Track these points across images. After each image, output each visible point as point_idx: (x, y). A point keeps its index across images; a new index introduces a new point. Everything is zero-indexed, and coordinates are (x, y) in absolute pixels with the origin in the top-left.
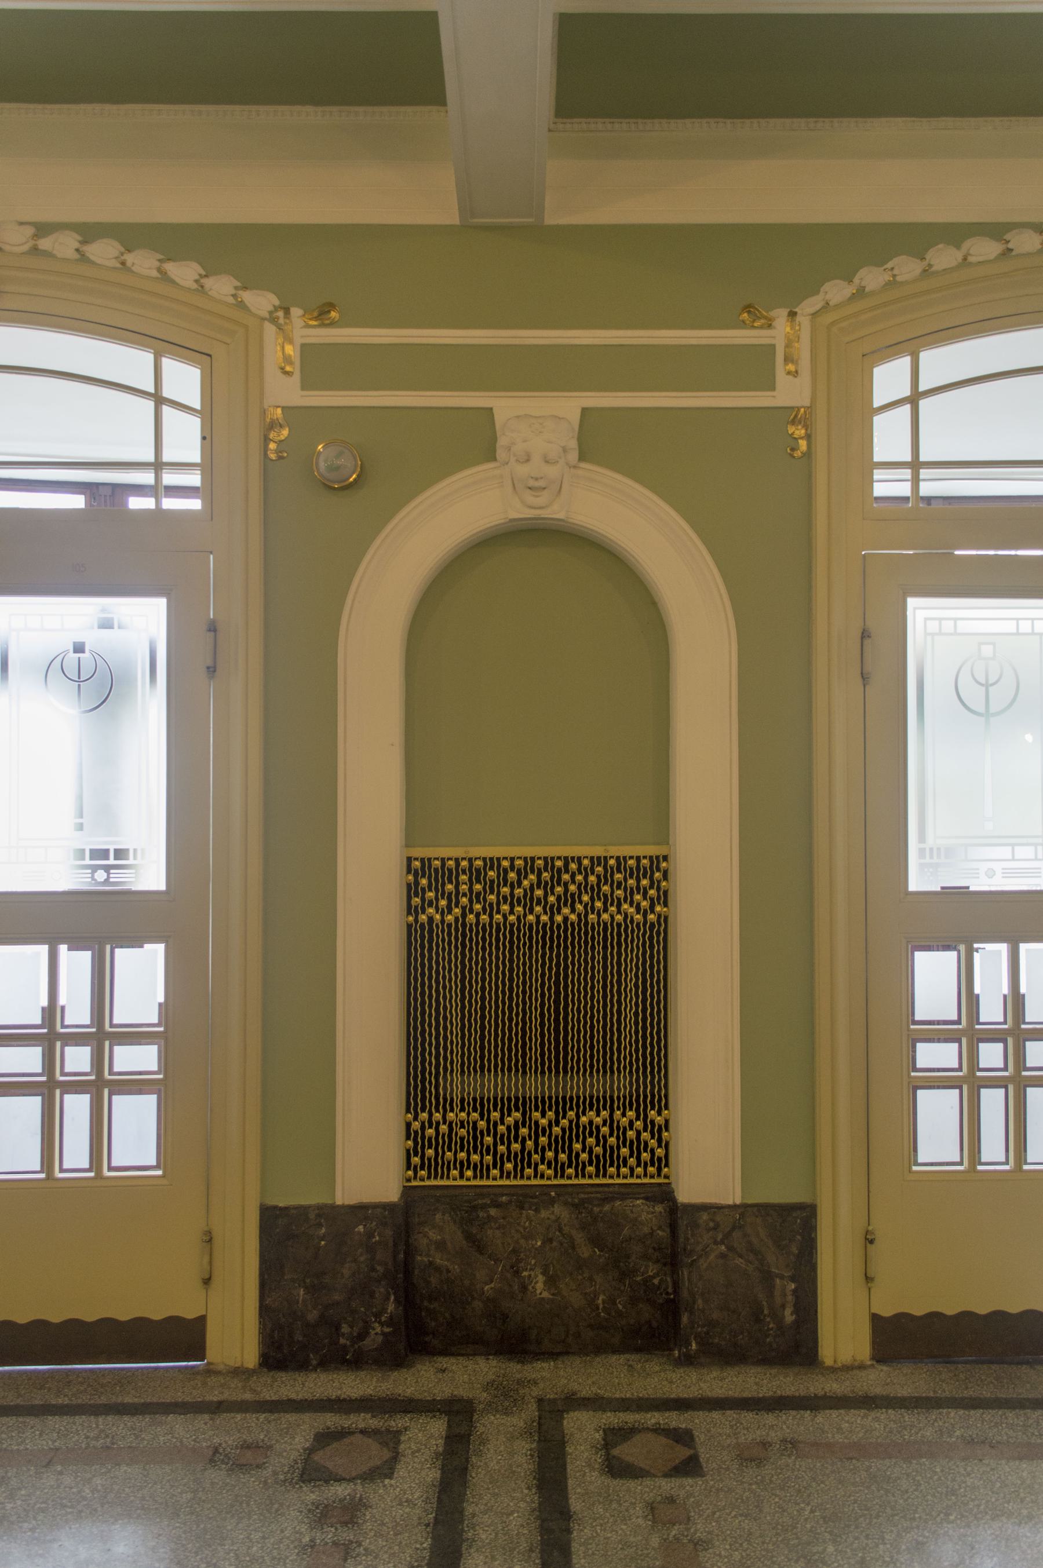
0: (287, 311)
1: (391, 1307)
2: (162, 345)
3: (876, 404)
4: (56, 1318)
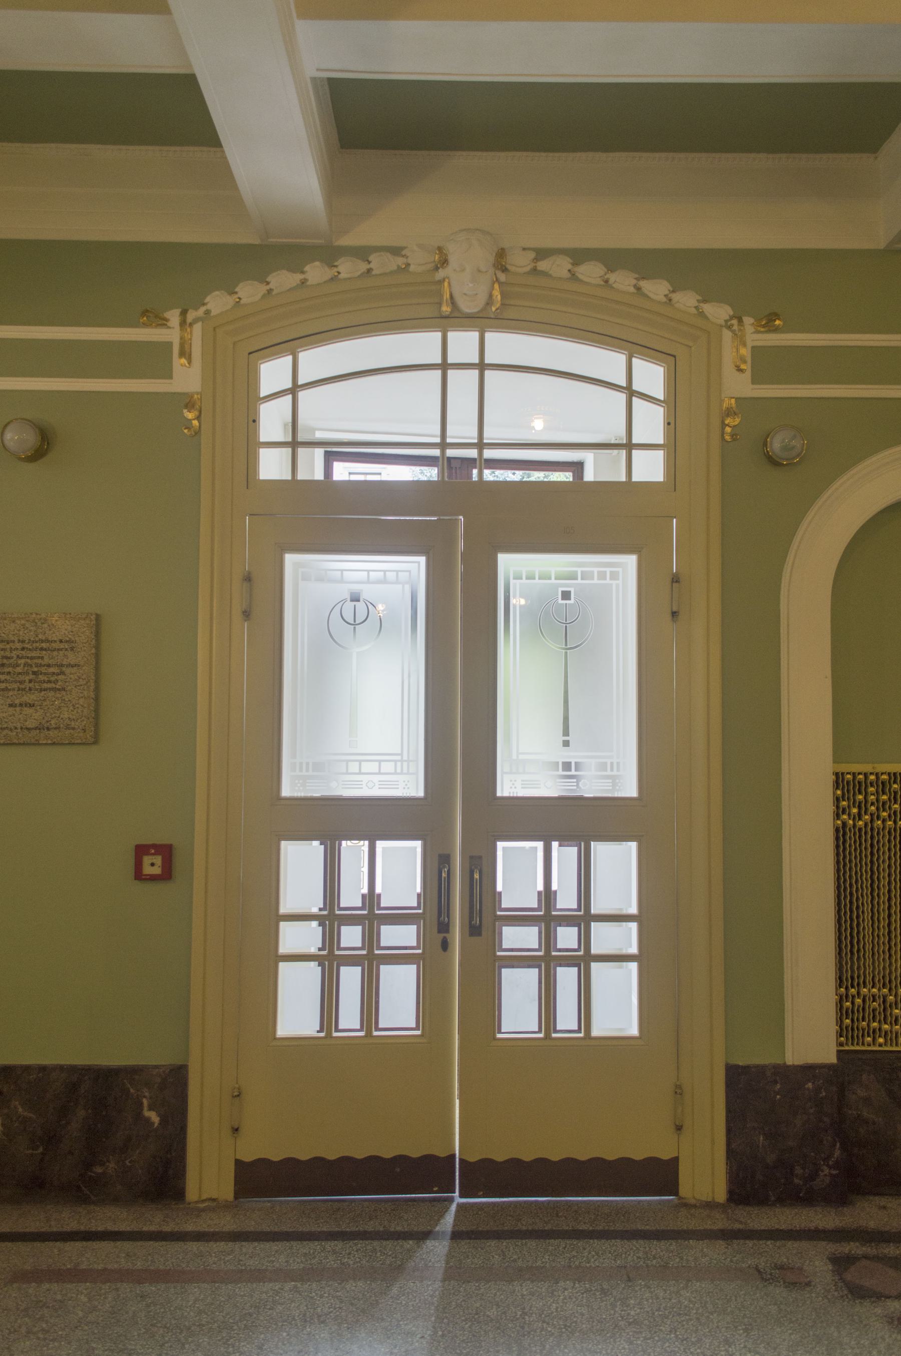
0: (740, 321)
1: (837, 1153)
2: (634, 347)
3: (263, 394)
4: (360, 1155)
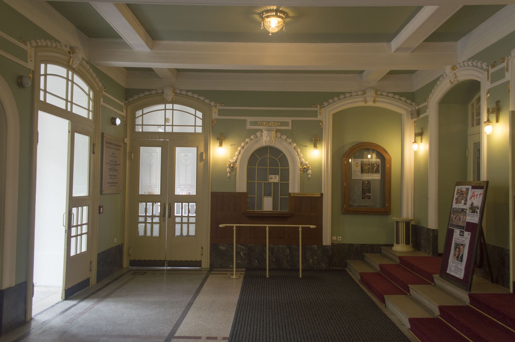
2: (196, 109)
